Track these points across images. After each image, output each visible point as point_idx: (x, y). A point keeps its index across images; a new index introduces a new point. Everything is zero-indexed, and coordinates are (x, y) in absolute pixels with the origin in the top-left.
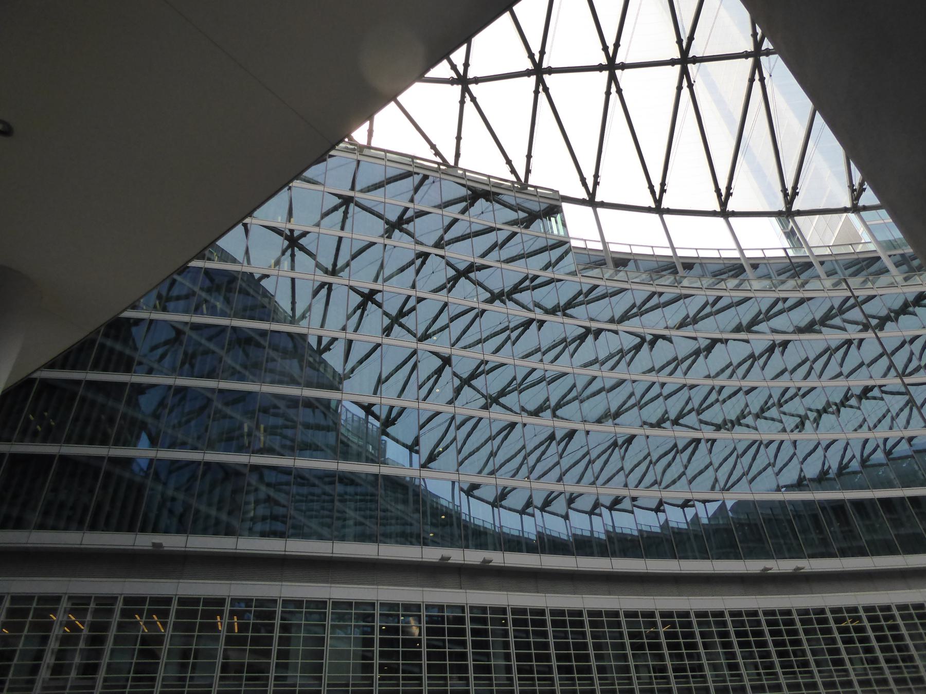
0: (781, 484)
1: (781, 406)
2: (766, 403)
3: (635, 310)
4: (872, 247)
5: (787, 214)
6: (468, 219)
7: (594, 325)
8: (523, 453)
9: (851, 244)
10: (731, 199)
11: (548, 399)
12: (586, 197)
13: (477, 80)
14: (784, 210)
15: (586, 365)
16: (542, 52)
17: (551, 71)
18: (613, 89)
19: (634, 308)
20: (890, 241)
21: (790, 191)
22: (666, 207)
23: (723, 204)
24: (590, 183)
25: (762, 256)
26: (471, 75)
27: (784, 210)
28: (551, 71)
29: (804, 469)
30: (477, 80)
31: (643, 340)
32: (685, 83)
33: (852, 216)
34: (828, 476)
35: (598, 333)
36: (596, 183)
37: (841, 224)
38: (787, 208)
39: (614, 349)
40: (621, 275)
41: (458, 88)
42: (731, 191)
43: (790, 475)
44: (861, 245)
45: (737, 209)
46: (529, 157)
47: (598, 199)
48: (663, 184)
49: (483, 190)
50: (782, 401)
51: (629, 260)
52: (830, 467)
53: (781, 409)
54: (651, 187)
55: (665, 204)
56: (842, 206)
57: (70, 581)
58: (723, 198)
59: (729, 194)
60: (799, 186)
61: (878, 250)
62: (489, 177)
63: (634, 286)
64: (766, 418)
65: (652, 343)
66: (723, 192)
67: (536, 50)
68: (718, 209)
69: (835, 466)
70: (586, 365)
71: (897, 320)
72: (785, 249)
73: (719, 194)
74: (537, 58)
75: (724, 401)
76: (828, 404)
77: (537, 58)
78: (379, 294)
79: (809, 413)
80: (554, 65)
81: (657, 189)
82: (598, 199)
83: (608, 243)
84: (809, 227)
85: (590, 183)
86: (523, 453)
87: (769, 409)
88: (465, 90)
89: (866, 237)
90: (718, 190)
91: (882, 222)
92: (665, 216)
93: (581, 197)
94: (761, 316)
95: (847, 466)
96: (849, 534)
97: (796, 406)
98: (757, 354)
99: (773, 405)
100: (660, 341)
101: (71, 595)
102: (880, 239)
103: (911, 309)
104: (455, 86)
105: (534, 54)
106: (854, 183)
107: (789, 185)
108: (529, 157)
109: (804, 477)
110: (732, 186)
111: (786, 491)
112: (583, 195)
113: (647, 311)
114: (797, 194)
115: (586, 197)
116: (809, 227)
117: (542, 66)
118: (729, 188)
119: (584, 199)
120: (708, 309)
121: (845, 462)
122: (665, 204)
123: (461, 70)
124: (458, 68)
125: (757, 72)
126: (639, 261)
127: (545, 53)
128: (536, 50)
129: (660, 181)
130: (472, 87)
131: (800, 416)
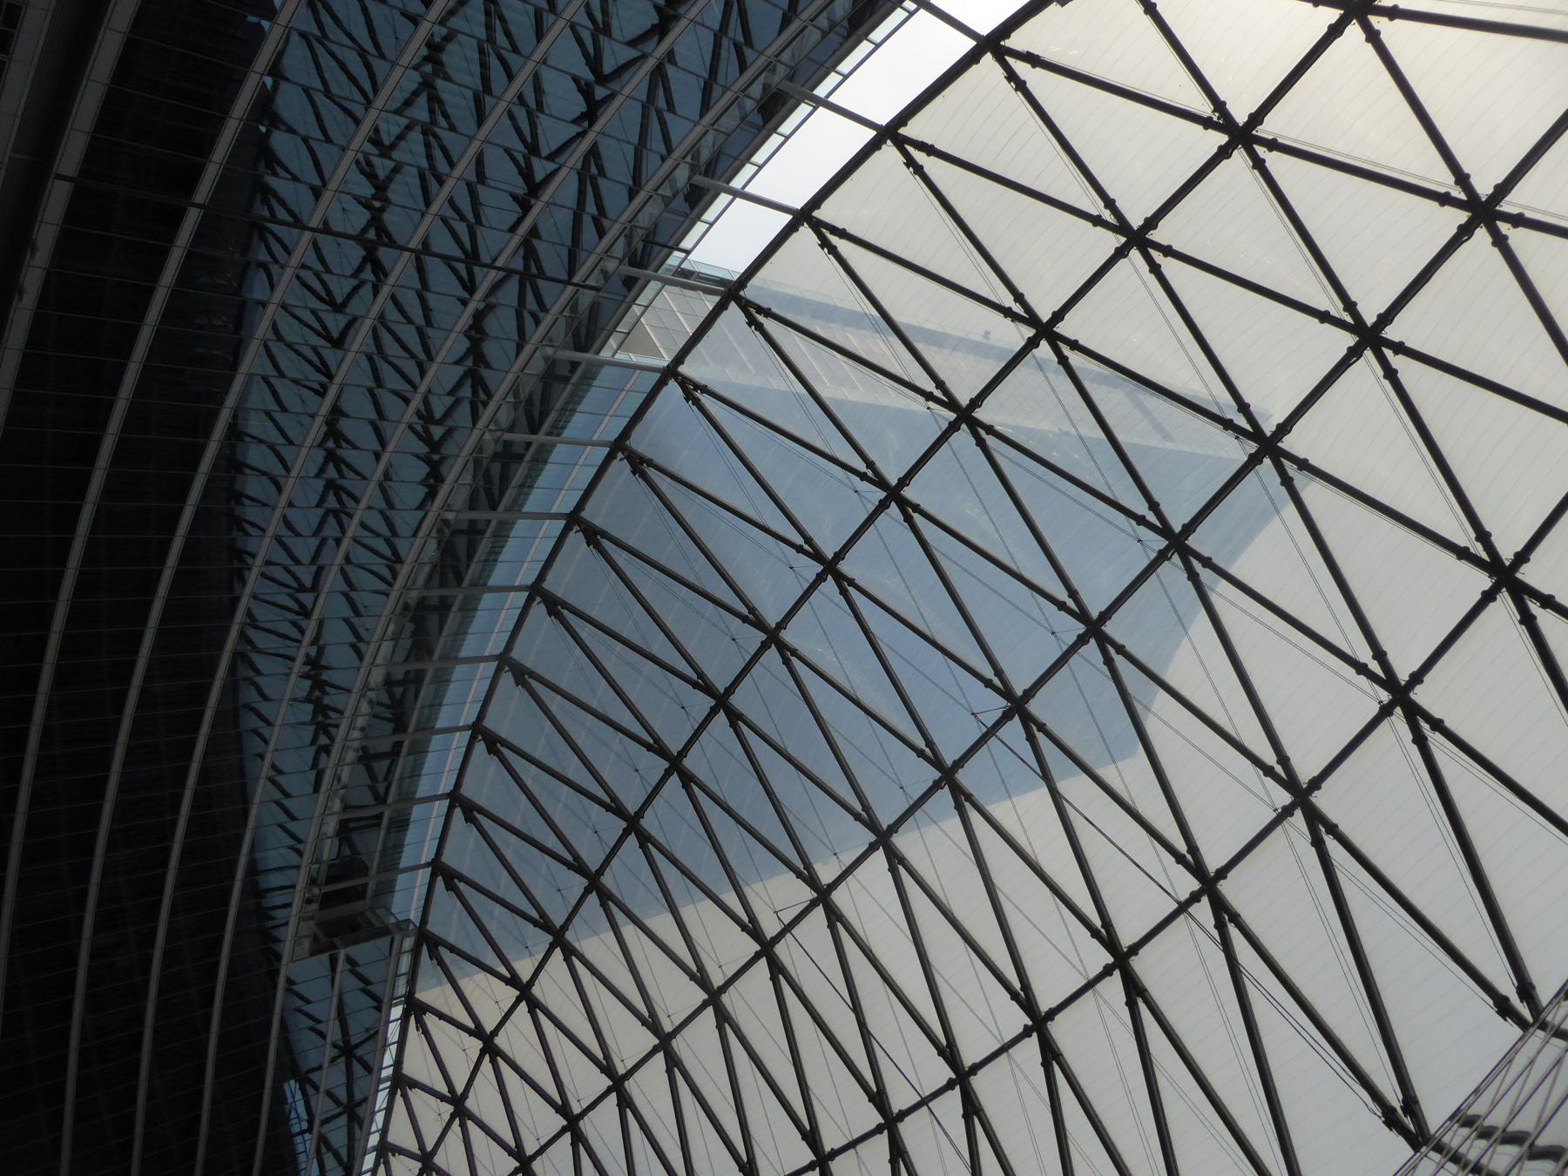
0: (284, 85)
1: (424, 133)
2: (446, 116)
3: (661, 103)
4: (605, 354)
5: (731, 292)
7: (538, 207)
8: (320, 98)
9: (628, 334)
10: (901, 159)
11: (447, 78)
12: (1007, 43)
14: (742, 293)
15: (479, 161)
16: (1155, 269)
19: (537, 268)
20: (594, 379)
21: (698, 394)
22: (884, 147)
23: (818, 226)
24: (1021, 68)
25: (780, 130)
27: (742, 293)
29: (290, 135)
31: (602, 79)
33: (664, 361)
34: (263, 164)
35: (525, 207)
36: (1011, 76)
37: (658, 345)
38: (742, 298)
39: (486, 213)
40: (756, 90)
42: (826, 250)
43: (290, 104)
44: (615, 347)
45: (794, 238)
47: (988, 58)
48: (919, 170)
49: (256, 791)
50: (432, 139)
51: (692, 208)
52: (275, 174)
53: (418, 128)
54: (930, 150)
55: (889, 151)
56: (688, 359)
58: (753, 311)
59: (825, 244)
60: (694, 408)
61: (597, 357)
63: (699, 129)
64: (416, 94)
65: (585, 91)
66: (834, 240)
67: (1169, 266)
68: (816, 214)
69: (272, 182)
70: (479, 161)
71: (468, 337)
72: (688, 252)
73: (760, 310)
74: (1156, 255)
75: (481, 51)
76: (387, 201)
77: (1156, 255)
78: (434, 401)
79: (390, 164)
80: (1122, 263)
81: (920, 156)
82: (988, 58)
83: (815, 109)
84: (691, 308)
85: (1021, 68)
86: (320, 98)
87: (431, 111)
89: (621, 356)
90: (843, 234)
91: (627, 388)
92: (872, 133)
93: (1015, 35)
94: (594, 170)
95: (266, 201)
97: (412, 151)
98: (602, 38)
99: (434, 122)
101: (6, 66)
102: (606, 370)
103: (469, 363)
107: (770, 325)
109: (277, 128)
110: (757, 333)
111: (264, 85)
112: (1016, 41)
113: (645, 116)
114: (750, 324)
115: (1007, 43)
116: (691, 308)
117: (1139, 249)
118: (833, 251)
119: (1008, 37)
121: (274, 202)
122: (889, 151)
126: (682, 219)
128: (1169, 266)
131: (393, 146)
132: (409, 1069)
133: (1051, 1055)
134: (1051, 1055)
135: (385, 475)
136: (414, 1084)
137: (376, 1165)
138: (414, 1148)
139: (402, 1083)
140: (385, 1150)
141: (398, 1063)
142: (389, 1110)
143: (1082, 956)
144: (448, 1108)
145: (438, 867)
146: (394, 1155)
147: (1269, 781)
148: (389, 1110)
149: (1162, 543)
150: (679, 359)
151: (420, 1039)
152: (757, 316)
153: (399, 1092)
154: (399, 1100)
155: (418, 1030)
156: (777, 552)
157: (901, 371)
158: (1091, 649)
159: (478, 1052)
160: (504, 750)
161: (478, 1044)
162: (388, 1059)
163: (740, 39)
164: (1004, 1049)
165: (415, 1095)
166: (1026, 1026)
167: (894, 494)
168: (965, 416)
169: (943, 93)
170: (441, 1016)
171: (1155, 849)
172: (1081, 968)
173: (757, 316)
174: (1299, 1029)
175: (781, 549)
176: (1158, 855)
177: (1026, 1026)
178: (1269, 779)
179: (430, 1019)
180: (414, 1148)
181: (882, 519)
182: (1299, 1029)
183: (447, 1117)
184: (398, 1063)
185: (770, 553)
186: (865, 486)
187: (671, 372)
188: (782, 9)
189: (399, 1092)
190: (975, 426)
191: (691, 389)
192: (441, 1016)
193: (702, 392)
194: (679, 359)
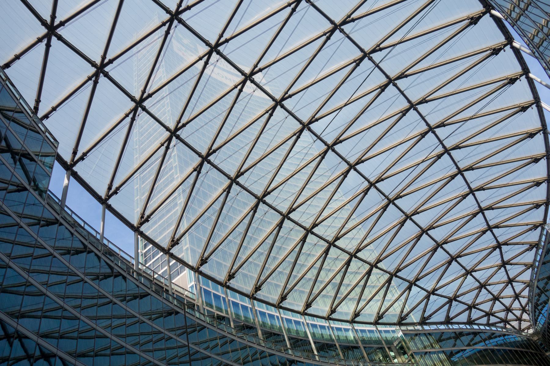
6: (7, 125)
10: (114, 197)
13: (60, 38)
17: (106, 75)
18: (131, 116)
21: (145, 217)
26: (60, 31)
28: (106, 75)
30: (60, 38)
32: (166, 145)
41: (43, 31)
46: (54, 109)
47: (75, 169)
55: (111, 202)
57: (157, 310)
60: (151, 217)
62: (21, 96)
73: (110, 188)
82: (75, 169)
88: (48, 36)
96: (502, 356)
100: (121, 277)
104: (43, 27)
105: (106, 58)
106: (175, 237)
108: (54, 109)
110: (121, 189)
114: (148, 221)
120: (11, 188)
123: (57, 22)
124: (56, 20)
125: (207, 56)
127: (112, 63)
129: (85, 150)
130: (54, 39)
132: (442, 319)
133: (402, 76)
134: (402, 76)
135: (149, 320)
136: (448, 316)
137: (475, 324)
138: (467, 312)
139: (448, 321)
140: (470, 322)
141: (441, 323)
142: (458, 323)
143: (415, 121)
144: (454, 303)
145: (376, 323)
146: (471, 319)
147: (297, 10)
148: (458, 323)
149: (214, 54)
150: (162, 249)
151: (433, 317)
152: (145, 218)
153: (451, 321)
154: (454, 320)
155: (430, 319)
156: (202, 179)
157: (158, 161)
158: (257, 77)
159: (434, 296)
160: (334, 307)
161: (432, 296)
162: (442, 327)
163: (211, 346)
164: (402, 93)
165: (452, 315)
166: (413, 110)
167: (205, 159)
168: (174, 133)
169: (88, 183)
170: (424, 311)
171: (326, 48)
172: (490, 198)
173: (145, 218)
174: (413, 28)
175: (201, 177)
176: (328, 46)
177: (413, 110)
178: (297, 10)
179: (426, 315)
180: (467, 312)
181: (216, 163)
182: (413, 28)
183: (457, 303)
184: (441, 323)
185: (203, 181)
186: (203, 171)
187: (196, 270)
188: (70, 257)
189: (451, 321)
190: (177, 129)
191: (144, 219)
192: (424, 311)
193: (144, 214)
194: (162, 249)
